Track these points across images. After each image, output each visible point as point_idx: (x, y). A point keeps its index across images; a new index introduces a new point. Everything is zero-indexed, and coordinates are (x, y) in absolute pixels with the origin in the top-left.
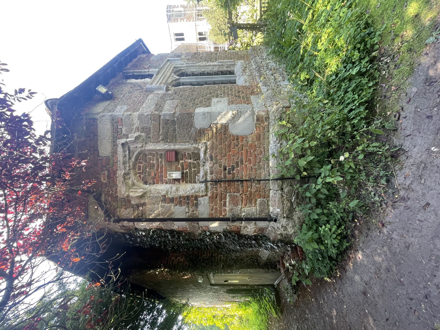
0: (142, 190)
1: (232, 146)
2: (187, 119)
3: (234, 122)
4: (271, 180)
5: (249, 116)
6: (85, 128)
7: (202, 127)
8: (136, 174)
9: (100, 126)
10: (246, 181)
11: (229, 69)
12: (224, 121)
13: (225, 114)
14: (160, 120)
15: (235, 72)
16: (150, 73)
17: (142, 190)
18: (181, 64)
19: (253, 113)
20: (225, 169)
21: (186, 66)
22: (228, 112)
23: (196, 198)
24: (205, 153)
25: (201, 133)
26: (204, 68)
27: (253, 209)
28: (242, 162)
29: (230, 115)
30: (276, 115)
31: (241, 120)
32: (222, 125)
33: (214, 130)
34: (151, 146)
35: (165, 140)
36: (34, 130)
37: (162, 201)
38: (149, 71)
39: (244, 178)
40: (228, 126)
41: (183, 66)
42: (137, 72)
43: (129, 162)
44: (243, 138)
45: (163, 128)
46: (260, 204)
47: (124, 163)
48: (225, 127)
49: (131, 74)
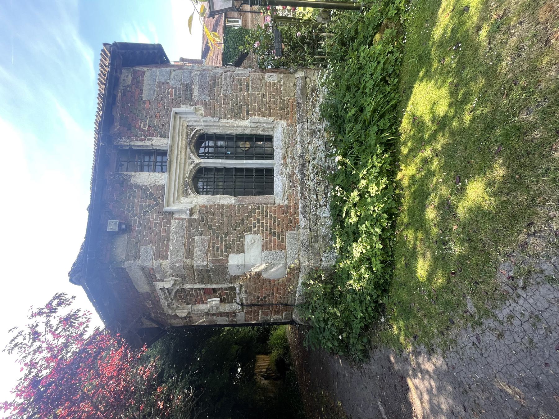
0: (186, 310)
1: (265, 285)
2: (221, 270)
3: (267, 271)
4: (297, 306)
5: (281, 267)
6: (114, 275)
7: (236, 274)
8: (178, 300)
9: (131, 274)
10: (276, 304)
11: (266, 133)
12: (257, 270)
13: (259, 266)
14: (193, 270)
15: (275, 139)
16: (155, 148)
17: (186, 310)
18: (196, 121)
19: (286, 264)
20: (259, 298)
21: (205, 126)
22: (261, 264)
23: (234, 313)
24: (240, 290)
25: (236, 278)
26: (231, 130)
27: (280, 317)
28: (273, 294)
29: (263, 266)
30: (307, 269)
31: (273, 270)
32: (256, 273)
33: (249, 276)
34: (188, 286)
35: (202, 282)
36: (79, 310)
37: (205, 315)
38: (152, 145)
39: (274, 303)
40: (261, 273)
41: (200, 124)
42: (135, 146)
43: (170, 296)
44: (274, 281)
45: (198, 275)
46: (286, 314)
47: (166, 298)
48: (259, 274)
49: (128, 148)
